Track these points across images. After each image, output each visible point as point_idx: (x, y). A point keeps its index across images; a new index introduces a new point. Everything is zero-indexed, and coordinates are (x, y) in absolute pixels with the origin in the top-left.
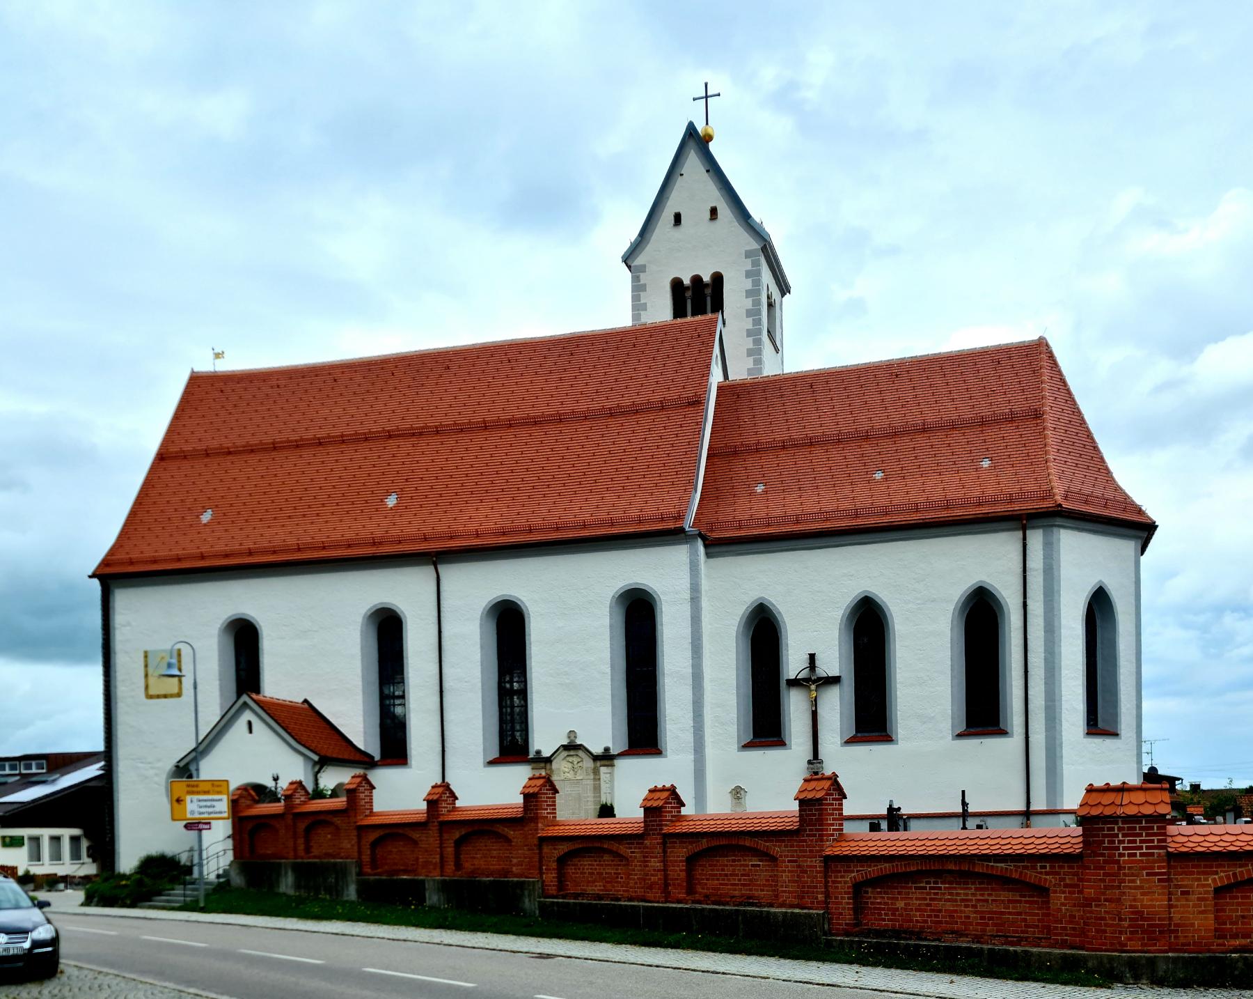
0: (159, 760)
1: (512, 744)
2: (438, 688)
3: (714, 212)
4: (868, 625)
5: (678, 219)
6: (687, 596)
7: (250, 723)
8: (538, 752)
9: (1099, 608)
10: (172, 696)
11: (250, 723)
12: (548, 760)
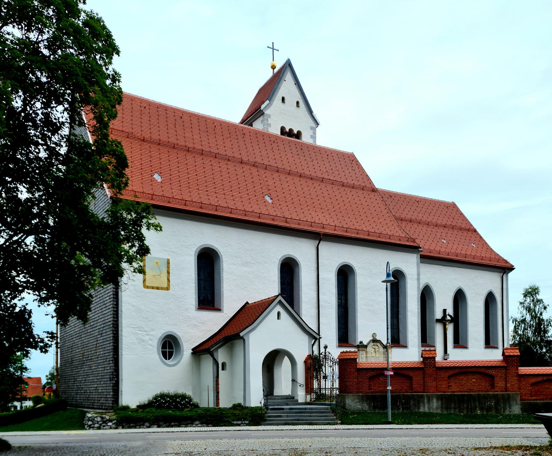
0: (153, 330)
1: (344, 337)
2: (315, 305)
3: (298, 103)
4: (459, 298)
5: (283, 99)
6: (416, 277)
7: (279, 314)
8: (361, 342)
9: (490, 299)
10: (162, 289)
11: (279, 314)
12: (366, 347)
